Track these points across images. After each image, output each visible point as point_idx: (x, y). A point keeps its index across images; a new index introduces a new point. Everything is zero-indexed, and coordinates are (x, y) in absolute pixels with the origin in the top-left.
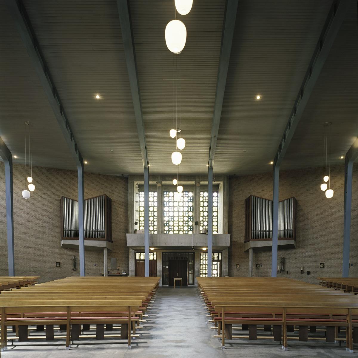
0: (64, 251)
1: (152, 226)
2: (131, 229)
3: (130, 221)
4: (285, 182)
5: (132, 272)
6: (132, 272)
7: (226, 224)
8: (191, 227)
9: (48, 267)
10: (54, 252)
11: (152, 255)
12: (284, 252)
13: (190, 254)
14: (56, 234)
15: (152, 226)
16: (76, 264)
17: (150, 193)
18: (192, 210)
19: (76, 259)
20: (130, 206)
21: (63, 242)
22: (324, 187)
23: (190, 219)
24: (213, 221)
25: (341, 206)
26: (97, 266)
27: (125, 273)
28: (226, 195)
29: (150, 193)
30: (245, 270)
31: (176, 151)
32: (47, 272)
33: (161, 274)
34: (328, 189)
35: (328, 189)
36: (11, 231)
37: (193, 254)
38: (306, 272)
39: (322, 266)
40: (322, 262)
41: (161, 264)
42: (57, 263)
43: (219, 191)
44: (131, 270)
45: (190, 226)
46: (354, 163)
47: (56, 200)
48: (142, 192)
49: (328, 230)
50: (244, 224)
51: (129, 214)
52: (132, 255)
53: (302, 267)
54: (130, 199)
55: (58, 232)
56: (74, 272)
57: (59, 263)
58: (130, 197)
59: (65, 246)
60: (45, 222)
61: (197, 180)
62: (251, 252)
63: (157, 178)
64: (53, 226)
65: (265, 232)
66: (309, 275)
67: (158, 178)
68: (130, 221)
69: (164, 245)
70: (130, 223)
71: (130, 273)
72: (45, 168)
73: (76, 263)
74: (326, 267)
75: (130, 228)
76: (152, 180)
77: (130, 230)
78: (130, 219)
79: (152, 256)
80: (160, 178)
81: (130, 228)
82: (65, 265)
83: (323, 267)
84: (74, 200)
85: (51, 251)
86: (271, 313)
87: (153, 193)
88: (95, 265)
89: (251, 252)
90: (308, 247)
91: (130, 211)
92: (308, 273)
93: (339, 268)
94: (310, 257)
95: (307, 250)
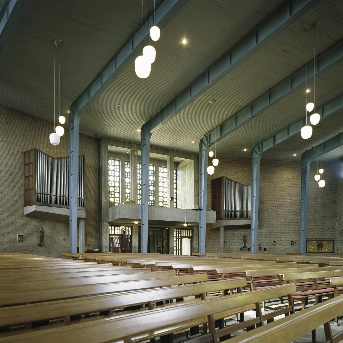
0: (29, 220)
1: (113, 197)
2: (105, 199)
3: (104, 189)
4: (245, 168)
5: (106, 248)
6: (106, 248)
7: (196, 201)
8: (152, 202)
9: (7, 241)
10: (14, 222)
11: (113, 229)
12: (245, 230)
13: (154, 229)
14: (18, 198)
15: (113, 197)
16: (43, 237)
17: (110, 161)
18: (152, 185)
19: (43, 231)
20: (104, 173)
21: (32, 209)
22: (317, 178)
23: (151, 193)
24: (119, 197)
25: (288, 194)
26: (66, 240)
27: (98, 250)
28: (196, 173)
29: (110, 161)
30: (212, 247)
31: (59, 125)
32: (5, 247)
33: (137, 251)
34: (321, 179)
35: (321, 179)
36: (207, 187)
37: (168, 229)
38: (263, 249)
39: (275, 243)
40: (275, 240)
41: (138, 239)
42: (19, 235)
43: (178, 169)
44: (104, 245)
45: (151, 201)
46: (312, 162)
47: (18, 152)
48: (112, 159)
49: (279, 213)
50: (210, 203)
51: (103, 181)
52: (106, 228)
53: (260, 244)
54: (104, 164)
55: (20, 194)
56: (40, 248)
57: (22, 236)
58: (104, 162)
59: (34, 215)
60: (4, 179)
61: (171, 154)
62: (222, 229)
63: (133, 146)
64: (14, 187)
65: (236, 212)
66: (266, 251)
67: (133, 145)
68: (104, 189)
69: (158, 219)
70: (104, 191)
71: (104, 250)
72: (4, 107)
73: (44, 236)
74: (277, 244)
75: (104, 198)
76: (121, 145)
77: (104, 200)
78: (104, 187)
79: (113, 231)
80: (136, 146)
81: (104, 198)
82: (29, 239)
83: (276, 245)
84: (49, 156)
85: (11, 220)
86: (313, 291)
87: (113, 161)
88: (64, 240)
89: (222, 229)
90: (264, 227)
91: (104, 178)
92: (265, 250)
93: (287, 246)
94: (266, 236)
95: (264, 229)
